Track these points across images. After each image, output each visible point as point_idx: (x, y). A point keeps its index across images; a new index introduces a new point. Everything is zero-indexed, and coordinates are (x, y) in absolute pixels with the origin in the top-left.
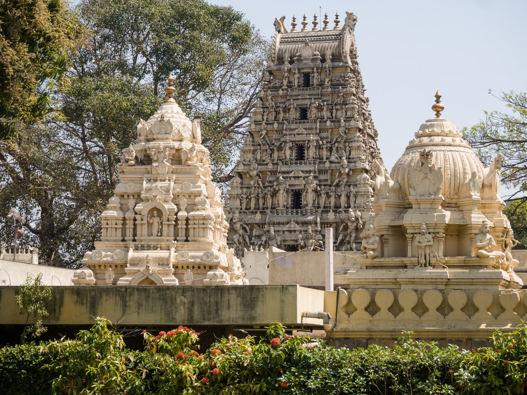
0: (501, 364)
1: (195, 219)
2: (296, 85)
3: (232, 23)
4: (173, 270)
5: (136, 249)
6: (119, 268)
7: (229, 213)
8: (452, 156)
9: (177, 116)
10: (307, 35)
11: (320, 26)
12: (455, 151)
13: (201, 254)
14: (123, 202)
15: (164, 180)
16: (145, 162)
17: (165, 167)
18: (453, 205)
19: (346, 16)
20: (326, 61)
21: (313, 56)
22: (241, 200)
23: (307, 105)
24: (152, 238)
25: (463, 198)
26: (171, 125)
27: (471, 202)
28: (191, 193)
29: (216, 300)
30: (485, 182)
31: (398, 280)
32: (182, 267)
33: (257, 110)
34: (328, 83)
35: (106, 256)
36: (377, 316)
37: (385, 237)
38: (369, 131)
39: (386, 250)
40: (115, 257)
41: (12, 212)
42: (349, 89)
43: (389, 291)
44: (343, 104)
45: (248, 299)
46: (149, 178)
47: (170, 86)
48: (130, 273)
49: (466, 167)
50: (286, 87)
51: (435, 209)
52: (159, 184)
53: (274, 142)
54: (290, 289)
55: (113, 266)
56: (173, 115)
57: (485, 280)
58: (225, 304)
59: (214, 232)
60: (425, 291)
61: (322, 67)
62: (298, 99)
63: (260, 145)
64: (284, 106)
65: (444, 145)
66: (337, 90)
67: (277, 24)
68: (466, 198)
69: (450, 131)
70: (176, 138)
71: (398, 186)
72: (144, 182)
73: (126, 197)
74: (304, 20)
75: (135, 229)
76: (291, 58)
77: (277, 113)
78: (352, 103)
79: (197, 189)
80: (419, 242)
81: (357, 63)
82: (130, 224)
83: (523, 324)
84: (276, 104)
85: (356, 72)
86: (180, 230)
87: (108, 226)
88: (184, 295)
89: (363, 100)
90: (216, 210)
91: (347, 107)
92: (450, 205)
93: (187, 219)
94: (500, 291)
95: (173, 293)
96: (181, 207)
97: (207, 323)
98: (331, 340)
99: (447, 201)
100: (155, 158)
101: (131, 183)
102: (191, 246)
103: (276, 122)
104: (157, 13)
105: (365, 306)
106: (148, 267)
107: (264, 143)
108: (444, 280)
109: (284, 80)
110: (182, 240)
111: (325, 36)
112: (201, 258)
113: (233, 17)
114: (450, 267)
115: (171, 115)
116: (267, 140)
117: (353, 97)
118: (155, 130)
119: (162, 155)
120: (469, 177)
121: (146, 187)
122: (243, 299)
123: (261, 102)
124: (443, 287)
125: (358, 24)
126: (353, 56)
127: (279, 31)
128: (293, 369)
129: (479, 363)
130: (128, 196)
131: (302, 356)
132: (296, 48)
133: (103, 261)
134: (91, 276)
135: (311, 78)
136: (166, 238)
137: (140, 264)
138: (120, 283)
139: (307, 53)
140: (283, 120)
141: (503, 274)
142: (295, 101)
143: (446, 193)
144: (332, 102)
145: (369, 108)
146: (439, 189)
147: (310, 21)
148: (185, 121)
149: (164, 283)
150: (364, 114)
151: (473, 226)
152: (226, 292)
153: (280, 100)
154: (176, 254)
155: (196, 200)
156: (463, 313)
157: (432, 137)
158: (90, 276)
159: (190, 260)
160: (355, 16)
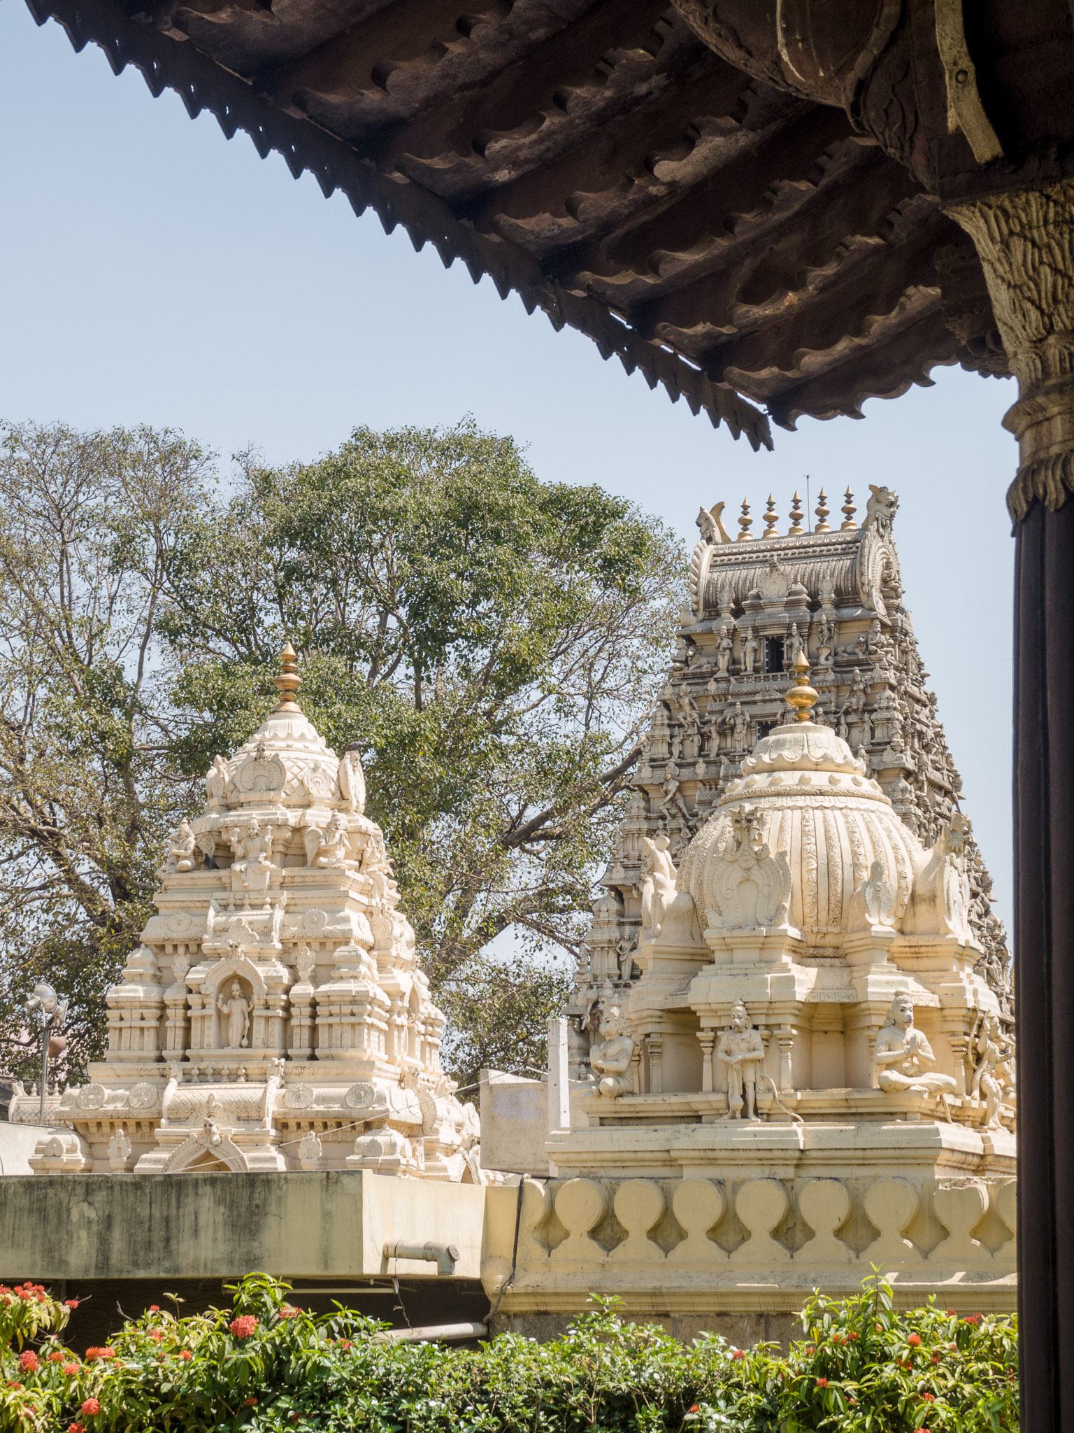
0: (810, 1390)
1: (331, 1003)
2: (750, 669)
3: (603, 526)
4: (273, 1132)
5: (187, 1080)
6: (145, 1129)
7: (591, 987)
8: (825, 820)
9: (299, 745)
10: (777, 546)
11: (809, 522)
12: (833, 808)
13: (342, 1090)
14: (163, 961)
15: (261, 906)
16: (218, 863)
17: (263, 874)
18: (830, 952)
19: (871, 493)
20: (820, 606)
21: (790, 594)
22: (619, 955)
23: (775, 715)
24: (226, 1051)
25: (852, 932)
26: (281, 769)
27: (869, 941)
28: (326, 937)
29: (165, 1213)
30: (918, 887)
31: (673, 1154)
32: (299, 1125)
33: (657, 733)
34: (827, 659)
35: (113, 1099)
36: (619, 1252)
37: (654, 1039)
38: (935, 776)
39: (656, 1074)
40: (135, 1103)
41: (40, 994)
42: (878, 673)
43: (650, 1184)
44: (864, 711)
45: (243, 1210)
46: (224, 902)
47: (287, 672)
48: (167, 1142)
49: (861, 850)
50: (726, 675)
51: (770, 963)
52: (247, 916)
53: (697, 808)
54: (346, 1180)
55: (132, 1124)
56: (290, 743)
57: (898, 1153)
58: (187, 1222)
59: (388, 1035)
60: (743, 1182)
61: (811, 623)
62: (755, 703)
63: (663, 818)
64: (720, 720)
65: (805, 794)
66: (850, 676)
67: (703, 521)
68: (858, 931)
69: (825, 757)
70: (295, 799)
71: (689, 905)
72: (211, 912)
73: (169, 949)
74: (770, 510)
75: (187, 1030)
76: (737, 601)
77: (705, 737)
78: (887, 708)
79: (339, 927)
80: (728, 1053)
81: (899, 609)
82: (175, 1018)
83: (876, 1274)
84: (701, 716)
85: (895, 631)
86: (296, 1031)
87: (122, 1024)
88: (90, 1199)
89: (918, 701)
90: (393, 978)
91: (874, 716)
92: (821, 951)
93: (314, 1004)
94: (939, 1181)
95: (63, 1195)
96: (300, 973)
97: (141, 1274)
98: (503, 1317)
99: (812, 940)
100: (238, 850)
101: (182, 915)
102: (321, 1071)
103: (701, 760)
104: (412, 505)
105: (590, 1224)
106: (208, 1126)
107: (673, 811)
108: (789, 1154)
109: (720, 657)
110: (300, 1057)
111: (819, 546)
112: (342, 1100)
113: (604, 509)
114: (808, 1117)
115: (283, 744)
116: (682, 805)
117: (888, 693)
118: (245, 782)
119: (257, 842)
120: (865, 875)
121: (216, 924)
122: (231, 1211)
123: (666, 713)
124: (789, 1172)
125: (900, 514)
126: (890, 589)
127: (710, 540)
128: (284, 1403)
129: (769, 1386)
130: (175, 947)
131: (309, 1365)
132: (735, 579)
133: (105, 1113)
134: (75, 1151)
135: (784, 649)
136: (262, 1052)
137: (192, 1119)
138: (142, 1167)
139: (773, 589)
140: (718, 755)
141: (942, 1136)
142: (746, 708)
143: (808, 920)
144: (837, 707)
145: (939, 719)
146: (780, 909)
147: (783, 510)
148: (320, 758)
149: (249, 1166)
150: (921, 735)
151: (871, 1005)
152: (190, 1190)
153: (711, 705)
154: (283, 1091)
155: (336, 954)
156: (841, 1243)
157: (776, 774)
158: (72, 1150)
159: (317, 1108)
160: (892, 494)
